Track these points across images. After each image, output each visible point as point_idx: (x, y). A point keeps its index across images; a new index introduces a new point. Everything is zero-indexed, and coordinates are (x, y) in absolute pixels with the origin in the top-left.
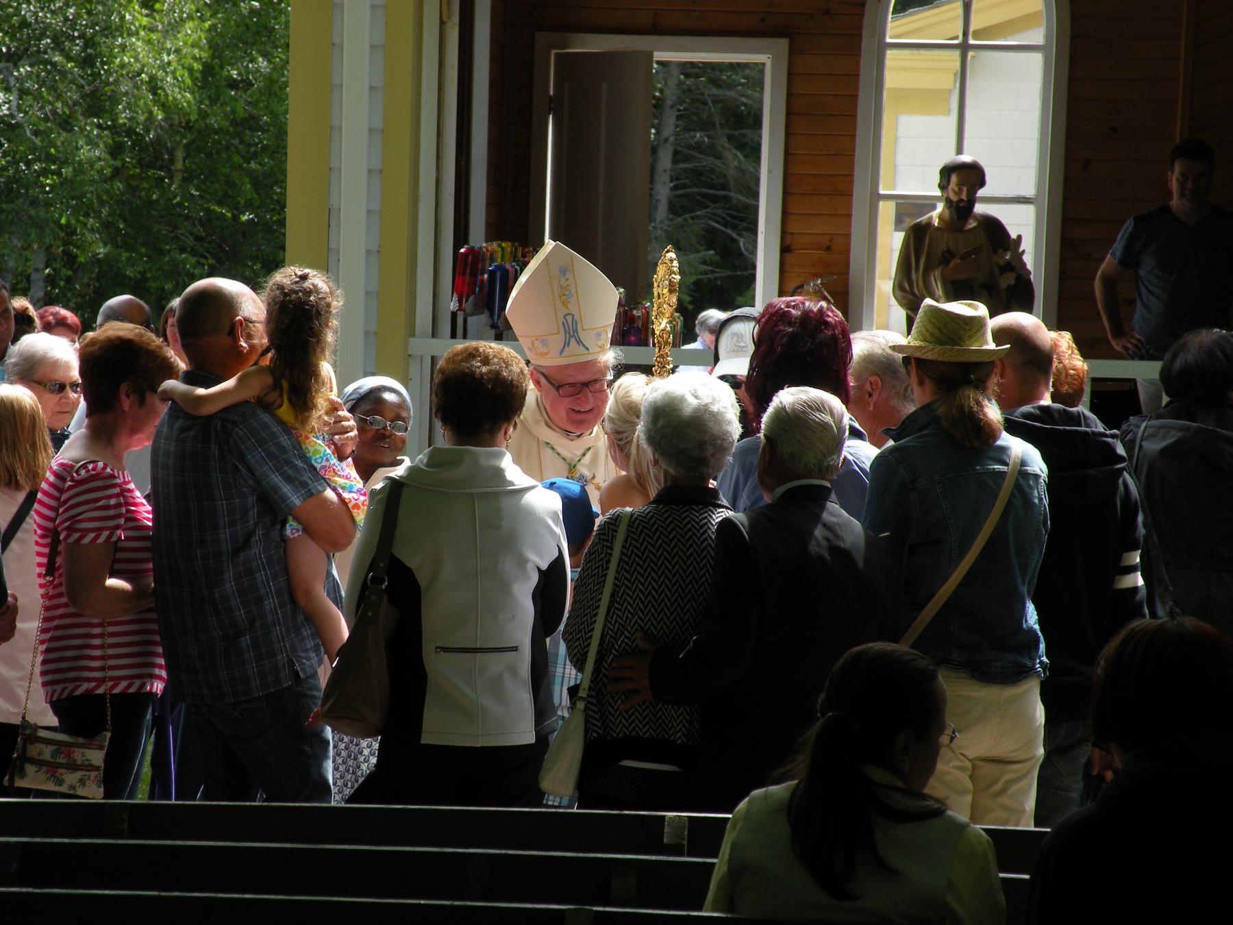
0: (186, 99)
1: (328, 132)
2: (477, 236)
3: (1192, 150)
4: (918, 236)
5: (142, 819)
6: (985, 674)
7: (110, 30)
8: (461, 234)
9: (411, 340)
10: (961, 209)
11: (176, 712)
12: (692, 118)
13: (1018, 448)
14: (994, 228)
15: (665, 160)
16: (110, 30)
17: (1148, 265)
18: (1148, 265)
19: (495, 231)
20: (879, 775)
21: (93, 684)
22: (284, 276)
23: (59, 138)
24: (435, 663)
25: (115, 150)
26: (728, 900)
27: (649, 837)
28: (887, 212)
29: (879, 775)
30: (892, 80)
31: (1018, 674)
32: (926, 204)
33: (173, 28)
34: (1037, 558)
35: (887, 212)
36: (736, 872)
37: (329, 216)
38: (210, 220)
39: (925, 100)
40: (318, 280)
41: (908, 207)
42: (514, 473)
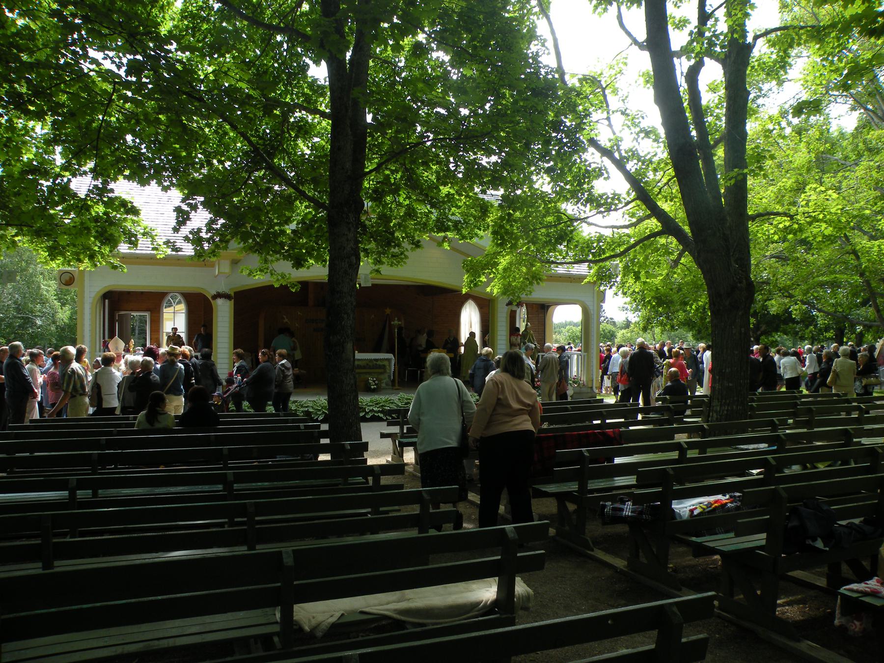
0: (67, 321)
1: (83, 325)
2: (107, 339)
3: (204, 326)
4: (169, 337)
5: (46, 421)
6: (176, 394)
7: (56, 312)
8: (104, 338)
9: (386, 423)
10: (175, 334)
11: (60, 408)
12: (141, 322)
13: (180, 365)
14: (179, 335)
15: (137, 328)
16: (56, 312)
17: (199, 340)
18: (199, 340)
19: (109, 338)
20: (158, 409)
21: (859, 595)
22: (78, 346)
23: (48, 327)
24: (104, 397)
25: (57, 329)
26: (138, 427)
27: (128, 419)
28: (165, 334)
29: (158, 409)
30: (165, 317)
31: (180, 394)
32: (170, 333)
33: (65, 312)
34: (182, 379)
35: (165, 334)
36: (139, 423)
37: (83, 336)
38: (71, 338)
39: (169, 320)
40: (83, 346)
41: (167, 333)
42: (114, 370)
